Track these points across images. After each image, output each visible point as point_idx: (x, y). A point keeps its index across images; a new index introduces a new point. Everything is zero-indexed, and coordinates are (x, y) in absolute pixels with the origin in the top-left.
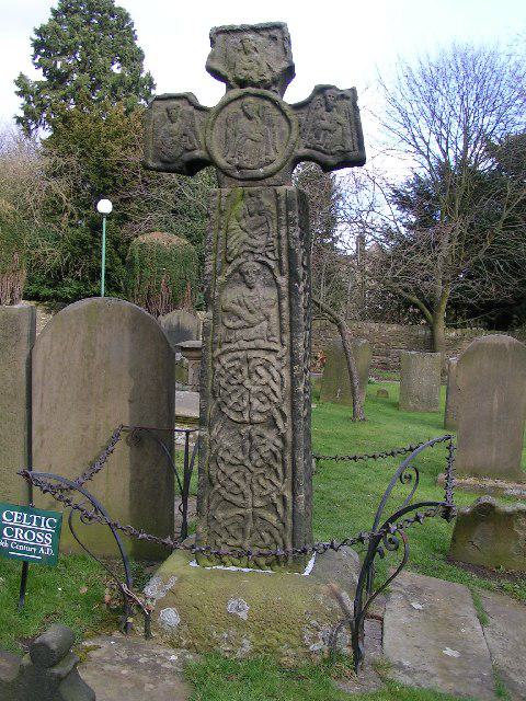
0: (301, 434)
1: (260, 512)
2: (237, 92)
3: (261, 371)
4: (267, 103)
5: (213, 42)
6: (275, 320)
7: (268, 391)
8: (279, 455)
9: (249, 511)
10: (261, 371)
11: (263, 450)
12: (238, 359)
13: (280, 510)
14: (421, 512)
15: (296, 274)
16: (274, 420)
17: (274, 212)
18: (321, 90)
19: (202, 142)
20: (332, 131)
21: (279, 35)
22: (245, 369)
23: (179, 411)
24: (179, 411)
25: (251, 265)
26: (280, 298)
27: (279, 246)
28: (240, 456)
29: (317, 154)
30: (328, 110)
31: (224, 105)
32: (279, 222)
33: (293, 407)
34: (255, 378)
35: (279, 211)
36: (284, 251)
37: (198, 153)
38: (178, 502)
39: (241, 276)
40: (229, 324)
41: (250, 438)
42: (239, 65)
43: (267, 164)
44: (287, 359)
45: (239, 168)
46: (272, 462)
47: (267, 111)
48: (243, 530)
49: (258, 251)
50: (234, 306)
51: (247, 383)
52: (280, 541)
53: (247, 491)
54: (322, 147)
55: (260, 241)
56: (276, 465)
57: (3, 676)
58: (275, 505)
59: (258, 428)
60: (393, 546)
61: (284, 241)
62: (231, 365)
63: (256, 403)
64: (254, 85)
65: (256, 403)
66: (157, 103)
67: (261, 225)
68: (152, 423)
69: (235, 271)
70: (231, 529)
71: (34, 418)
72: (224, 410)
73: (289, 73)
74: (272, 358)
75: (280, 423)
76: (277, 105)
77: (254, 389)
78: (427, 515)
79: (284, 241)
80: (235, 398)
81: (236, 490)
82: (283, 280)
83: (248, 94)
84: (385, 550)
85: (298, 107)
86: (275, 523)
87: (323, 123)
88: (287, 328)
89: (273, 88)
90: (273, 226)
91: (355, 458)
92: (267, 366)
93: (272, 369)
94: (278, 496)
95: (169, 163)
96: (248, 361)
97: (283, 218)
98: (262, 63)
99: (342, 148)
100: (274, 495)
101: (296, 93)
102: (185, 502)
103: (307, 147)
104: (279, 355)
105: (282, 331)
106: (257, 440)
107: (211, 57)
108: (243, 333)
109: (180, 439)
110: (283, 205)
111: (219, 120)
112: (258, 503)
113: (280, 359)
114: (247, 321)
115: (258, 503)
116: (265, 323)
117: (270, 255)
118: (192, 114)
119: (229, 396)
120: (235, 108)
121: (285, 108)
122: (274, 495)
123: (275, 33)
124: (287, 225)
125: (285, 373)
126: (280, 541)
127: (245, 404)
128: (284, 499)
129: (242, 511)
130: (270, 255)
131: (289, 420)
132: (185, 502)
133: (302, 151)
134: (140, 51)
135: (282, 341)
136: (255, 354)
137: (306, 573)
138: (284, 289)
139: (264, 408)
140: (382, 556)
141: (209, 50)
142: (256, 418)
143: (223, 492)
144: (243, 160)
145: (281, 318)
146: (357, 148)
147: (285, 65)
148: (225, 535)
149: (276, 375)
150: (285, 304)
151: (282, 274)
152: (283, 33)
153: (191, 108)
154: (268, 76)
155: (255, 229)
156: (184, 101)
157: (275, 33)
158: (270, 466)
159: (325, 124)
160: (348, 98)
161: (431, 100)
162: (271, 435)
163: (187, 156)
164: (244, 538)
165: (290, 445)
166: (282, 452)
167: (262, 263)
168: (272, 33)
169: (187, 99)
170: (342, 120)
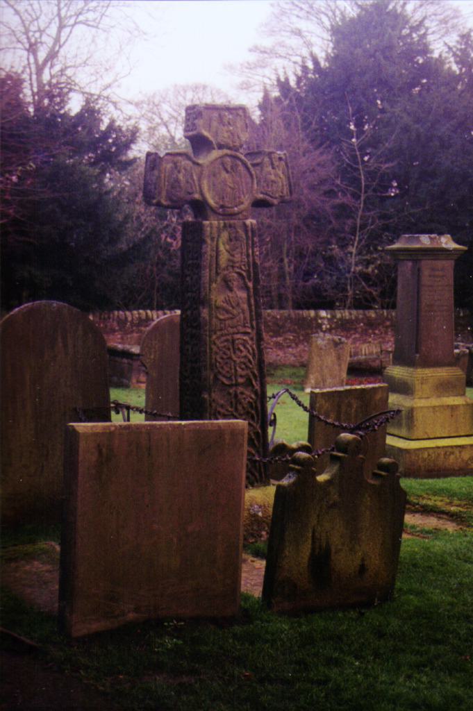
7: (246, 361)
16: (251, 380)
26: (249, 297)
32: (247, 244)
41: (236, 396)
54: (271, 194)
59: (240, 389)
62: (222, 345)
79: (251, 259)
82: (250, 285)
94: (254, 433)
105: (251, 320)
106: (240, 396)
110: (250, 234)
117: (243, 267)
119: (222, 368)
124: (257, 319)
131: (258, 379)
139: (244, 373)
149: (250, 349)
151: (250, 280)
166: (255, 402)
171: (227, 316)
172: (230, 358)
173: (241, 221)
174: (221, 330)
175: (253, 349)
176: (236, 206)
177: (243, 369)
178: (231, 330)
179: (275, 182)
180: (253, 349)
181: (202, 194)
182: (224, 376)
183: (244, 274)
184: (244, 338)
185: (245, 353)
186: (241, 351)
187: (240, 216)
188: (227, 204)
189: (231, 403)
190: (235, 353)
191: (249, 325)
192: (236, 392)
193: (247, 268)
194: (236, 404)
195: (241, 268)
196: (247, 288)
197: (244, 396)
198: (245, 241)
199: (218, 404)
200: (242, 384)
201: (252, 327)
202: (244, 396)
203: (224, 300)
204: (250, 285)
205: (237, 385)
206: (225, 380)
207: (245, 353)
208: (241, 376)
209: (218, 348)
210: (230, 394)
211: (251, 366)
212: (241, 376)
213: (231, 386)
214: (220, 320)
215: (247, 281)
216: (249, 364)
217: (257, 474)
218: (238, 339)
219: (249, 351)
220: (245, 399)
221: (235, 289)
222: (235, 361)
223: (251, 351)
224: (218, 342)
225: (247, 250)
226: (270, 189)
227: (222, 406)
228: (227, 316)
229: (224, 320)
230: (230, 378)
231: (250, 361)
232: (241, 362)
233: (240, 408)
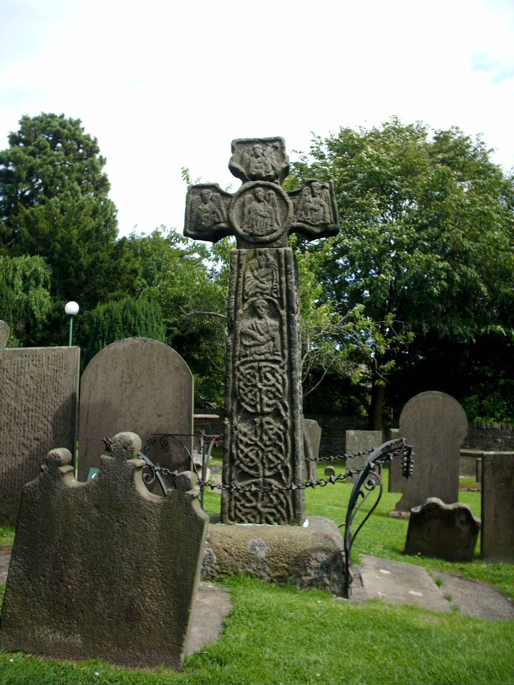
3: (269, 376)
7: (273, 389)
10: (269, 376)
25: (261, 302)
39: (254, 311)
41: (261, 425)
51: (260, 385)
90: (276, 275)
92: (273, 371)
112: (268, 473)
115: (268, 473)
128: (286, 469)
136: (264, 364)
142: (266, 409)
150: (285, 328)
157: (277, 144)
175: (283, 379)
185: (273, 381)
186: (269, 380)
200: (268, 414)
204: (283, 312)
207: (273, 381)
213: (256, 414)
216: (278, 394)
217: (284, 511)
218: (265, 367)
219: (277, 381)
226: (308, 217)
230: (254, 407)
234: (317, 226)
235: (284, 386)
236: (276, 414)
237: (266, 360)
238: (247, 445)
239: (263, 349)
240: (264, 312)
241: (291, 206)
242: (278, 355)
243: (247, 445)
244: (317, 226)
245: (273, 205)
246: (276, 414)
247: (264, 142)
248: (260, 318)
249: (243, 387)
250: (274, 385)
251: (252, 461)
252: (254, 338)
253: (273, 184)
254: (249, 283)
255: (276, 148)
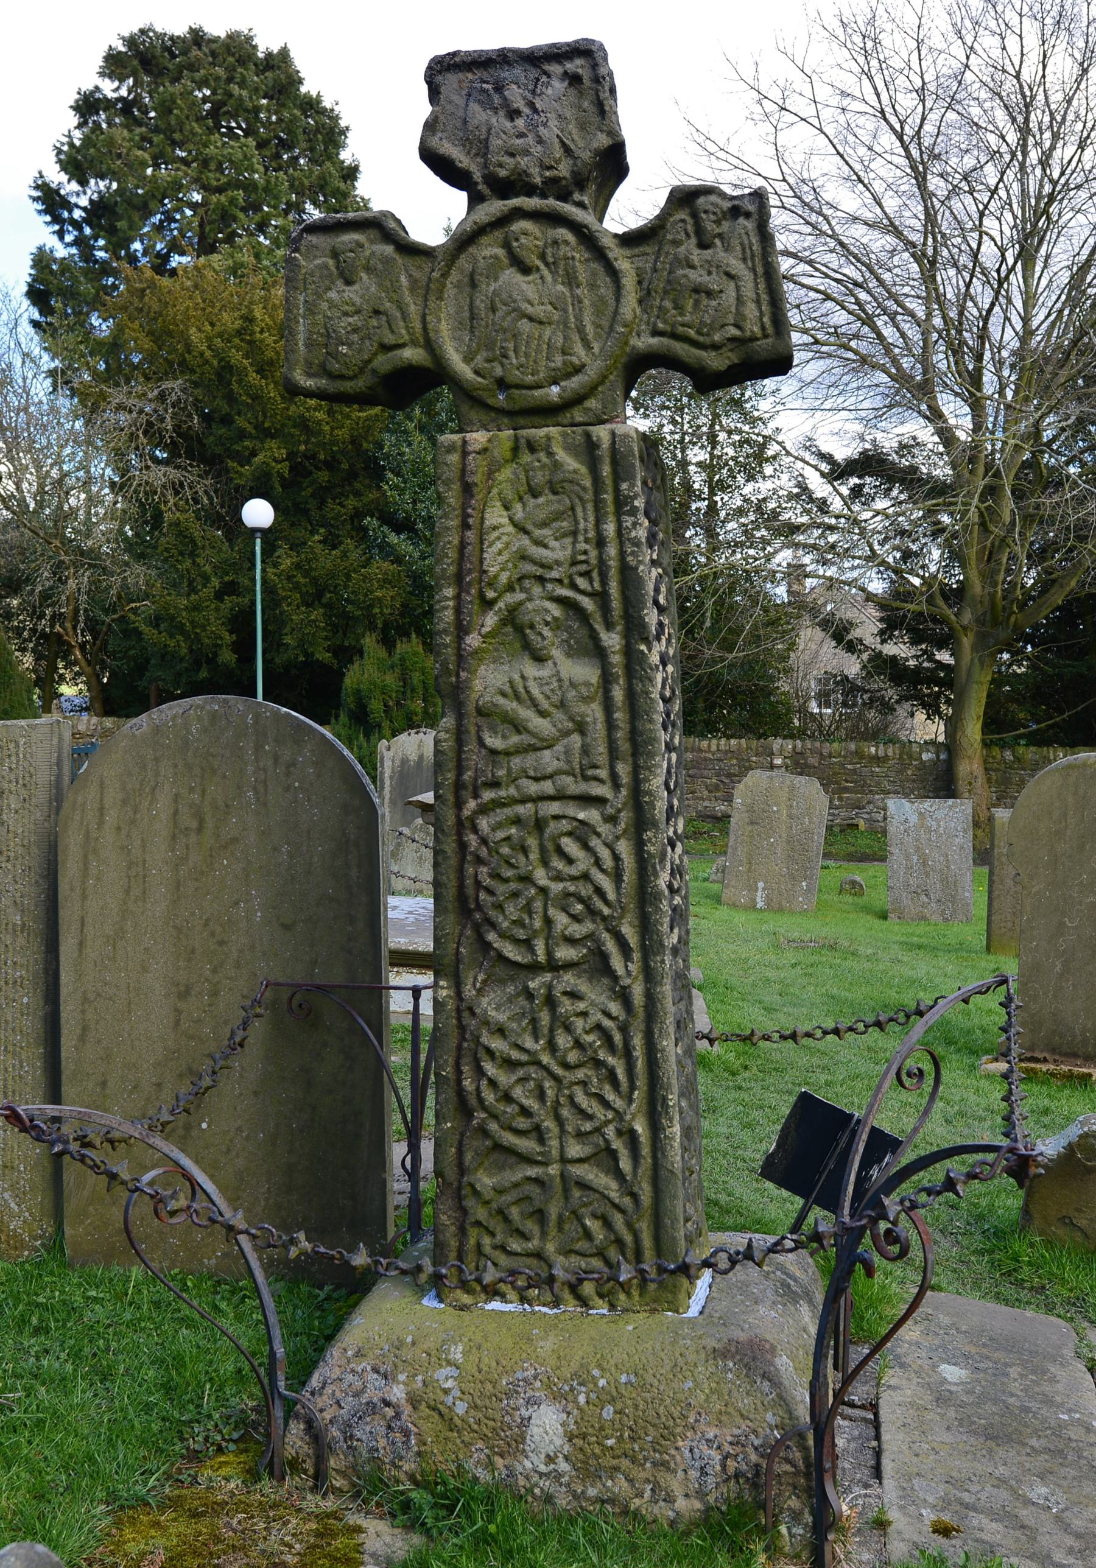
0: (667, 989)
1: (577, 1170)
2: (495, 207)
3: (570, 846)
4: (564, 233)
5: (434, 94)
6: (599, 729)
7: (586, 890)
8: (617, 1038)
9: (554, 1170)
10: (570, 846)
11: (579, 1024)
12: (517, 821)
13: (625, 1164)
14: (956, 1166)
15: (643, 626)
16: (604, 957)
17: (587, 483)
18: (685, 199)
19: (418, 326)
20: (714, 296)
21: (585, 74)
22: (532, 842)
23: (396, 940)
24: (396, 940)
25: (542, 608)
26: (607, 679)
27: (602, 564)
28: (529, 1043)
29: (680, 349)
30: (703, 245)
31: (464, 240)
32: (598, 504)
33: (646, 926)
34: (558, 864)
35: (597, 480)
36: (613, 573)
37: (412, 354)
38: (398, 1151)
39: (517, 631)
40: (493, 741)
41: (550, 1002)
42: (496, 143)
43: (568, 376)
44: (625, 817)
45: (502, 384)
46: (602, 1055)
47: (564, 250)
48: (540, 1215)
49: (555, 574)
50: (501, 700)
51: (541, 876)
52: (628, 1238)
53: (549, 1124)
54: (692, 333)
55: (558, 551)
56: (611, 1060)
57: (43, 530)
58: (613, 1154)
59: (569, 979)
60: (895, 1249)
61: (612, 551)
62: (500, 835)
63: (561, 920)
64: (530, 190)
65: (561, 920)
66: (313, 239)
67: (558, 516)
68: (337, 976)
69: (503, 622)
70: (514, 1212)
71: (66, 978)
72: (491, 937)
73: (612, 165)
74: (590, 815)
75: (617, 963)
76: (588, 239)
77: (556, 887)
78: (971, 1176)
79: (612, 551)
80: (512, 910)
81: (522, 1123)
82: (612, 640)
83: (519, 213)
84: (876, 1258)
85: (630, 239)
86: (614, 1195)
87: (693, 275)
88: (624, 746)
89: (577, 196)
90: (586, 522)
91: (793, 1036)
92: (582, 833)
93: (594, 842)
94: (619, 1133)
95: (342, 377)
96: (540, 825)
97: (608, 497)
98: (550, 130)
99: (736, 332)
100: (610, 1131)
101: (632, 206)
102: (414, 1148)
103: (656, 333)
104: (610, 811)
105: (613, 754)
106: (566, 1006)
107: (430, 126)
108: (529, 761)
109: (399, 1003)
110: (606, 470)
111: (454, 276)
112: (575, 1150)
113: (612, 819)
114: (533, 735)
115: (575, 1150)
116: (576, 739)
117: (582, 583)
118: (386, 261)
119: (500, 907)
120: (489, 249)
121: (607, 242)
122: (610, 1131)
123: (581, 68)
124: (618, 513)
125: (624, 848)
126: (628, 1238)
127: (538, 924)
128: (631, 1137)
129: (532, 1172)
130: (582, 583)
131: (636, 956)
132: (414, 1148)
133: (645, 342)
134: (233, 37)
135: (614, 776)
136: (555, 808)
137: (694, 1311)
138: (616, 659)
139: (578, 930)
140: (870, 1272)
141: (424, 109)
142: (564, 953)
143: (493, 1126)
144: (513, 369)
145: (611, 726)
146: (770, 330)
147: (603, 141)
148: (499, 1228)
149: (605, 854)
150: (618, 694)
151: (609, 626)
152: (595, 66)
153: (389, 249)
154: (564, 170)
155: (544, 524)
156: (373, 233)
157: (576, 65)
158: (598, 1064)
159: (696, 276)
160: (748, 215)
161: (921, 180)
162: (596, 996)
163: (383, 363)
164: (544, 1234)
165: (641, 1012)
166: (624, 1029)
167: (560, 601)
168: (569, 66)
169: (327, 133)
170: (736, 265)
171: (515, 739)
172: (527, 879)
173: (579, 430)
174: (495, 784)
175: (616, 858)
176: (556, 383)
177: (575, 918)
178: (533, 788)
179: (709, 294)
180: (616, 858)
181: (430, 345)
182: (502, 935)
183: (587, 603)
184: (581, 816)
187: (578, 415)
188: (515, 376)
189: (534, 1021)
190: (545, 863)
191: (603, 773)
192: (550, 987)
193: (597, 585)
194: (551, 1030)
195: (573, 586)
196: (600, 653)
197: (582, 1006)
198: (589, 496)
199: (487, 1023)
200: (569, 966)
201: (616, 785)
202: (582, 1006)
203: (507, 688)
204: (612, 640)
205: (554, 967)
206: (511, 952)
207: (583, 862)
208: (571, 941)
209: (484, 841)
210: (530, 996)
211: (606, 911)
212: (571, 941)
213: (534, 968)
214: (493, 752)
215: (599, 627)
216: (599, 904)
218: (556, 817)
219: (598, 863)
220: (584, 1014)
221: (556, 653)
222: (543, 891)
223: (608, 863)
224: (484, 824)
225: (598, 523)
226: (687, 318)
227: (501, 1031)
228: (515, 739)
229: (507, 753)
230: (527, 944)
231: (599, 891)
232: (567, 895)
233: (563, 1040)
234: (715, 347)
235: (617, 876)
236: (599, 966)
237: (560, 796)
238: (510, 1064)
239: (548, 760)
240: (548, 639)
241: (629, 282)
242: (596, 779)
243: (510, 1064)
244: (715, 347)
245: (571, 281)
246: (599, 966)
247: (537, 59)
248: (539, 658)
249: (487, 881)
250: (585, 876)
251: (525, 1112)
252: (518, 727)
253: (568, 208)
254: (499, 545)
255: (574, 80)
